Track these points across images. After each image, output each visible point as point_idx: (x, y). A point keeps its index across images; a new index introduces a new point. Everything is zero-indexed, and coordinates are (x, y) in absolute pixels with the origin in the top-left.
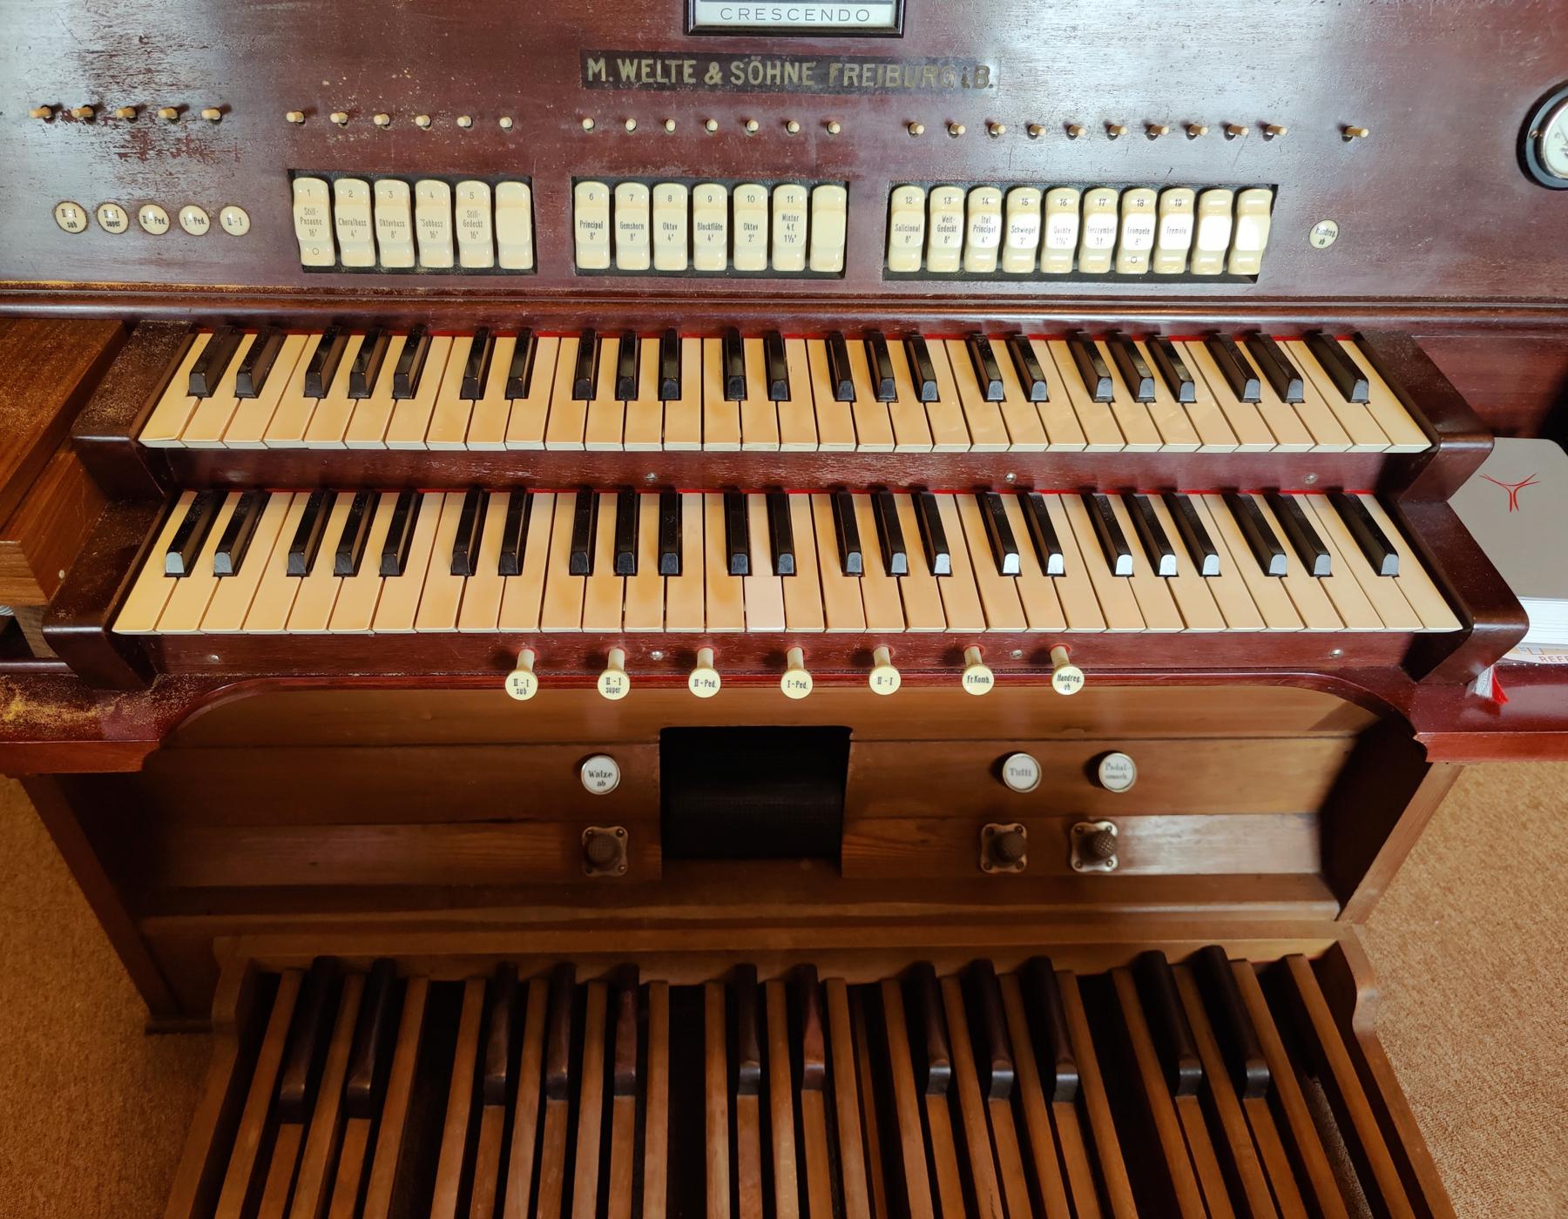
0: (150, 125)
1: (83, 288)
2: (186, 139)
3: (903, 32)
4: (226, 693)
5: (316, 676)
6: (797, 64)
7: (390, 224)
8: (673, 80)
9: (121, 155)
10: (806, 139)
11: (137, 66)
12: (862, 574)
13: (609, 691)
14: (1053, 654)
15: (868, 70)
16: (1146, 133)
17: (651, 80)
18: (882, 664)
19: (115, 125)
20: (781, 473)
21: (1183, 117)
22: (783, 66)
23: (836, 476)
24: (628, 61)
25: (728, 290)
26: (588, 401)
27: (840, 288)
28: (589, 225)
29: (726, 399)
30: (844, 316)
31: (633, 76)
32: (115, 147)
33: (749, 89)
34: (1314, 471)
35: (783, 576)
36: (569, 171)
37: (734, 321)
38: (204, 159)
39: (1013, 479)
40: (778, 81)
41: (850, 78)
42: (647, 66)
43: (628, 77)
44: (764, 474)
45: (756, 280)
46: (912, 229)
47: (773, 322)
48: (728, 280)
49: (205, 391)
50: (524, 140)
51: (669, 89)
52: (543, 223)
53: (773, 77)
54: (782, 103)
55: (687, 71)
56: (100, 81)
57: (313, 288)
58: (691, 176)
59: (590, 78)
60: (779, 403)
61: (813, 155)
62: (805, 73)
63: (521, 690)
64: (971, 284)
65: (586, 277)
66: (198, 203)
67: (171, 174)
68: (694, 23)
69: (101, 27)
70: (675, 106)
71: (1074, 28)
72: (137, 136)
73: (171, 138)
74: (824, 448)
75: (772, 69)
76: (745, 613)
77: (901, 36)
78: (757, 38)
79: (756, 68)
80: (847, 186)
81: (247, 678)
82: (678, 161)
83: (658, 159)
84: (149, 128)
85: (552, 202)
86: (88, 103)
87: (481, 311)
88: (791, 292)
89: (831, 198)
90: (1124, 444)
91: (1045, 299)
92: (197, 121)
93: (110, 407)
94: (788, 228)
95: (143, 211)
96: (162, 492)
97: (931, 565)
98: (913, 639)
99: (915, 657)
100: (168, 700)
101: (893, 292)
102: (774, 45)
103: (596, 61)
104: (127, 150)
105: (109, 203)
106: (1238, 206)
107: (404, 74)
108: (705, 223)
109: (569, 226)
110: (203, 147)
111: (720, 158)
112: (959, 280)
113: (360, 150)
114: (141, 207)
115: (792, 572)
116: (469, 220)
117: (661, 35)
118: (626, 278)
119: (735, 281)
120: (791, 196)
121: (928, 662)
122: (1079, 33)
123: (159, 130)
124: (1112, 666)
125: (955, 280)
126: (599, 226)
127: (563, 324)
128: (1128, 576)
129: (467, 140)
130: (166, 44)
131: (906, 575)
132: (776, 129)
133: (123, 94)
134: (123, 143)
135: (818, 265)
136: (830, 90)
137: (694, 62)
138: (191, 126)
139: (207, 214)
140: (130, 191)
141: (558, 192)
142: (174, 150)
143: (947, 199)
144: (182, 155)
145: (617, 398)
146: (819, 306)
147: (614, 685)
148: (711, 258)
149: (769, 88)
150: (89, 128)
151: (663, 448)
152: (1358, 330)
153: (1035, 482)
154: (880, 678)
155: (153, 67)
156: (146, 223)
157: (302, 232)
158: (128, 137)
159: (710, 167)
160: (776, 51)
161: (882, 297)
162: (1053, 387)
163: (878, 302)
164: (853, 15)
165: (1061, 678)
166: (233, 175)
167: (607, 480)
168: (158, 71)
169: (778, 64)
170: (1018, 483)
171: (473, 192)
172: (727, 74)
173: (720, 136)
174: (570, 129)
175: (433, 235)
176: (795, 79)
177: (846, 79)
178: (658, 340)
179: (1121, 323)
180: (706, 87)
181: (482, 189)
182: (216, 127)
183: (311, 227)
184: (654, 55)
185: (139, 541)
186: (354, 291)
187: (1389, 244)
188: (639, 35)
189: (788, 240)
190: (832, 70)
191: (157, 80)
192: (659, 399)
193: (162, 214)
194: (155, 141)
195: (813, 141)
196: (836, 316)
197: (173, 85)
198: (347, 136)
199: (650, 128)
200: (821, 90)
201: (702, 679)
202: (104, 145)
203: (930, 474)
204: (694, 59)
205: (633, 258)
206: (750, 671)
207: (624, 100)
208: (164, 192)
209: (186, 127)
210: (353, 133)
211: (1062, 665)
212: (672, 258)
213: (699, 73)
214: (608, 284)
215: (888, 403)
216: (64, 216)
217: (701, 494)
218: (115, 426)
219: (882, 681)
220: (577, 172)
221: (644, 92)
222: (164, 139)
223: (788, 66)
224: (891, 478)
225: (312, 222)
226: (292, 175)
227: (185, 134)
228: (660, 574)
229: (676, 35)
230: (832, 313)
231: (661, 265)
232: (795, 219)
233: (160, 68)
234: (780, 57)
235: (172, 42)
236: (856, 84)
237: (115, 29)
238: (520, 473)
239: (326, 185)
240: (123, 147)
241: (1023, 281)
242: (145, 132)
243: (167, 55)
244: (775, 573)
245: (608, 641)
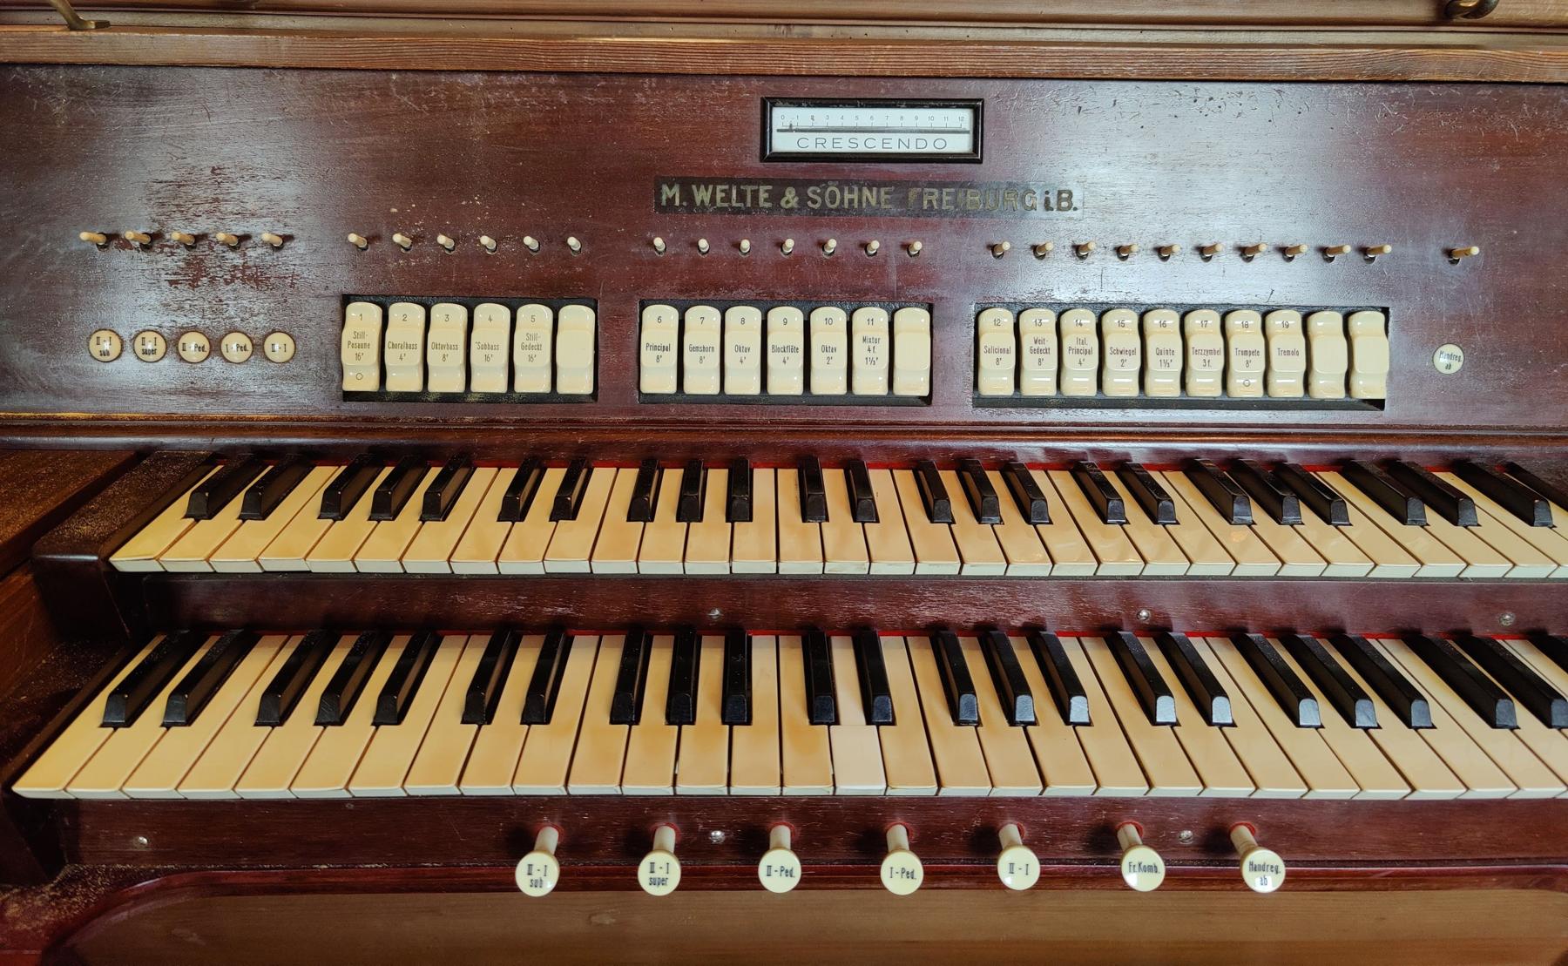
0: (207, 253)
1: (102, 419)
2: (243, 266)
3: (982, 157)
4: (150, 894)
5: (271, 868)
6: (875, 189)
7: (443, 347)
8: (749, 205)
9: (171, 282)
10: (886, 261)
11: (205, 195)
12: (978, 723)
13: (653, 882)
14: (1234, 836)
15: (948, 194)
16: (1241, 255)
17: (726, 205)
18: (1012, 844)
19: (171, 252)
20: (870, 608)
21: (1280, 242)
22: (860, 190)
23: (935, 614)
24: (702, 187)
25: (804, 419)
26: (645, 522)
27: (927, 415)
28: (655, 348)
29: (804, 520)
30: (933, 444)
31: (707, 200)
32: (167, 274)
33: (826, 212)
34: (1510, 609)
35: (878, 725)
36: (638, 294)
37: (812, 449)
38: (257, 285)
39: (1147, 618)
40: (856, 205)
41: (930, 202)
42: (722, 191)
43: (702, 201)
44: (849, 610)
45: (835, 407)
46: (1003, 351)
47: (855, 450)
48: (805, 407)
49: (205, 513)
50: (592, 263)
51: (744, 213)
52: (607, 347)
53: (851, 201)
54: (860, 226)
55: (763, 195)
56: (164, 210)
57: (351, 417)
58: (765, 299)
59: (664, 203)
60: (866, 525)
61: (893, 279)
62: (883, 197)
63: (536, 881)
64: (1070, 411)
65: (650, 405)
66: (243, 330)
67: (221, 301)
68: (771, 150)
69: (174, 158)
70: (749, 230)
71: (1155, 156)
72: (193, 264)
73: (228, 264)
74: (923, 569)
75: (849, 193)
76: (834, 775)
77: (980, 162)
78: (833, 164)
79: (833, 192)
80: (930, 309)
81: (182, 871)
82: (752, 284)
83: (731, 281)
84: (206, 255)
85: (617, 325)
86: (148, 231)
87: (532, 439)
88: (873, 419)
89: (914, 321)
90: (1147, 788)
91: (1154, 427)
92: (258, 248)
93: (87, 525)
94: (869, 350)
95: (184, 339)
96: (128, 631)
97: (1064, 712)
98: (1049, 812)
99: (1054, 840)
100: (70, 897)
101: (985, 420)
102: (851, 170)
103: (671, 187)
104: (180, 277)
105: (148, 330)
106: (1350, 329)
107: (474, 201)
108: (780, 346)
109: (634, 351)
110: (259, 274)
111: (796, 280)
112: (1057, 408)
113: (420, 274)
114: (183, 334)
115: (891, 720)
116: (527, 343)
117: (737, 162)
118: (694, 406)
119: (812, 408)
120: (871, 319)
121: (1072, 848)
122: (1160, 160)
123: (217, 257)
124: (1313, 857)
125: (1053, 407)
126: (666, 349)
127: (623, 452)
128: (1317, 728)
129: (532, 263)
130: (238, 175)
131: (1034, 724)
132: (854, 251)
133: (186, 223)
134: (176, 269)
135: (901, 389)
136: (910, 213)
137: (770, 187)
138: (251, 253)
139: (251, 341)
140: (174, 318)
141: (624, 316)
142: (228, 277)
143: (1038, 321)
144: (236, 281)
145: (678, 520)
146: (905, 432)
147: (659, 874)
148: (785, 382)
149: (847, 212)
150: (143, 255)
151: (729, 792)
152: (1510, 460)
153: (1173, 621)
154: (1012, 865)
155: (221, 197)
156: (184, 350)
157: (347, 356)
158: (182, 264)
159: (785, 290)
160: (853, 176)
161: (974, 424)
162: (1180, 509)
163: (970, 428)
164: (930, 144)
165: (1254, 868)
166: (285, 301)
167: (662, 618)
168: (226, 201)
169: (856, 188)
170: (1155, 623)
171: (535, 316)
172: (803, 199)
173: (796, 259)
174: (640, 253)
175: (487, 358)
176: (873, 202)
177: (925, 202)
178: (726, 471)
179: (1243, 451)
180: (782, 211)
181: (545, 313)
182: (276, 254)
183: (357, 351)
184: (730, 181)
185: (81, 684)
186: (395, 420)
187: (1522, 369)
188: (715, 163)
189: (869, 363)
190: (910, 194)
191: (222, 209)
192: (727, 521)
193: (203, 341)
194: (210, 268)
195: (893, 263)
196: (924, 443)
197: (239, 213)
198: (409, 261)
199: (725, 251)
200: (901, 214)
201: (776, 866)
202: (156, 272)
203: (1052, 610)
204: (770, 185)
205: (702, 382)
206: (839, 860)
207: (697, 223)
208: (209, 319)
209: (245, 254)
210: (415, 258)
211: (1250, 850)
212: (744, 383)
213: (776, 197)
214: (673, 412)
215: (992, 525)
216: (98, 344)
217: (774, 637)
218: (86, 545)
219: (1016, 870)
220: (646, 295)
221: (719, 217)
222: (220, 266)
223: (866, 191)
224: (1001, 615)
225: (360, 346)
226: (346, 300)
227: (242, 261)
228: (724, 723)
229: (753, 162)
230: (920, 439)
231: (732, 388)
232: (877, 341)
233: (227, 198)
234: (857, 183)
235: (244, 173)
236: (936, 207)
237: (189, 160)
238: (560, 610)
239: (381, 309)
240: (175, 274)
241: (1127, 408)
242: (202, 260)
243: (238, 185)
244: (869, 722)
245: (655, 814)
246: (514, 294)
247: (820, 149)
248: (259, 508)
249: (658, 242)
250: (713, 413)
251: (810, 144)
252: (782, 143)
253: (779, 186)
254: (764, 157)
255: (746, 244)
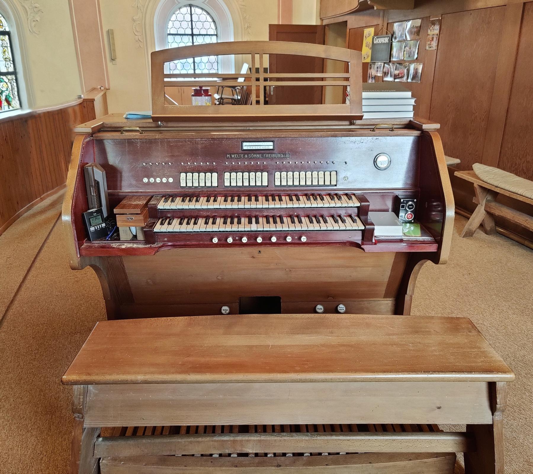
20: (257, 213)
55: (242, 156)
147: (230, 240)
148: (246, 184)
172: (248, 156)
173: (247, 165)
184: (237, 154)
213: (244, 156)
224: (276, 214)
229: (240, 151)
246: (205, 171)
247: (250, 149)
248: (173, 201)
249: (227, 163)
250: (236, 189)
251: (249, 148)
252: (245, 148)
253: (244, 154)
254: (242, 150)
255: (240, 163)
